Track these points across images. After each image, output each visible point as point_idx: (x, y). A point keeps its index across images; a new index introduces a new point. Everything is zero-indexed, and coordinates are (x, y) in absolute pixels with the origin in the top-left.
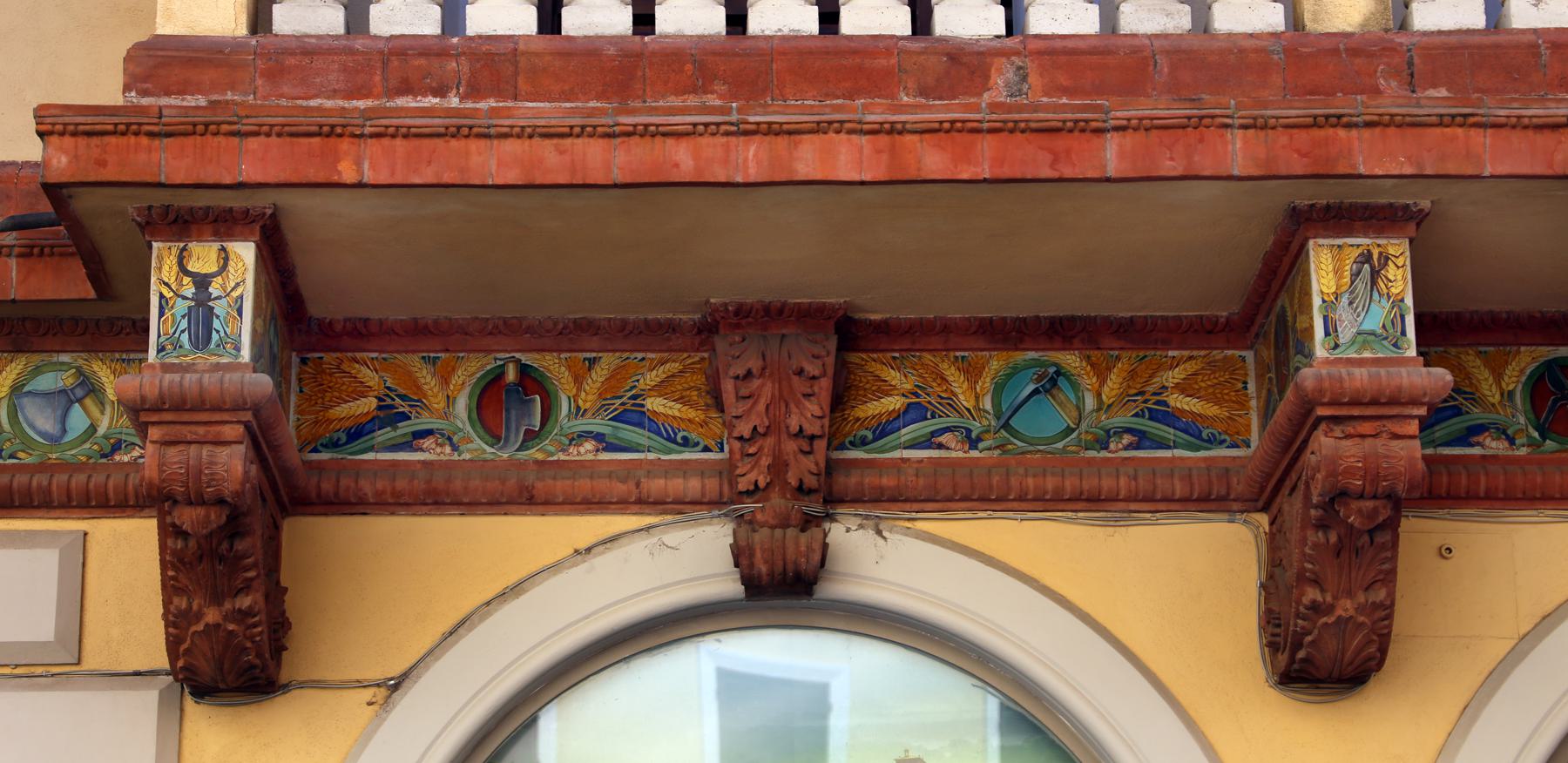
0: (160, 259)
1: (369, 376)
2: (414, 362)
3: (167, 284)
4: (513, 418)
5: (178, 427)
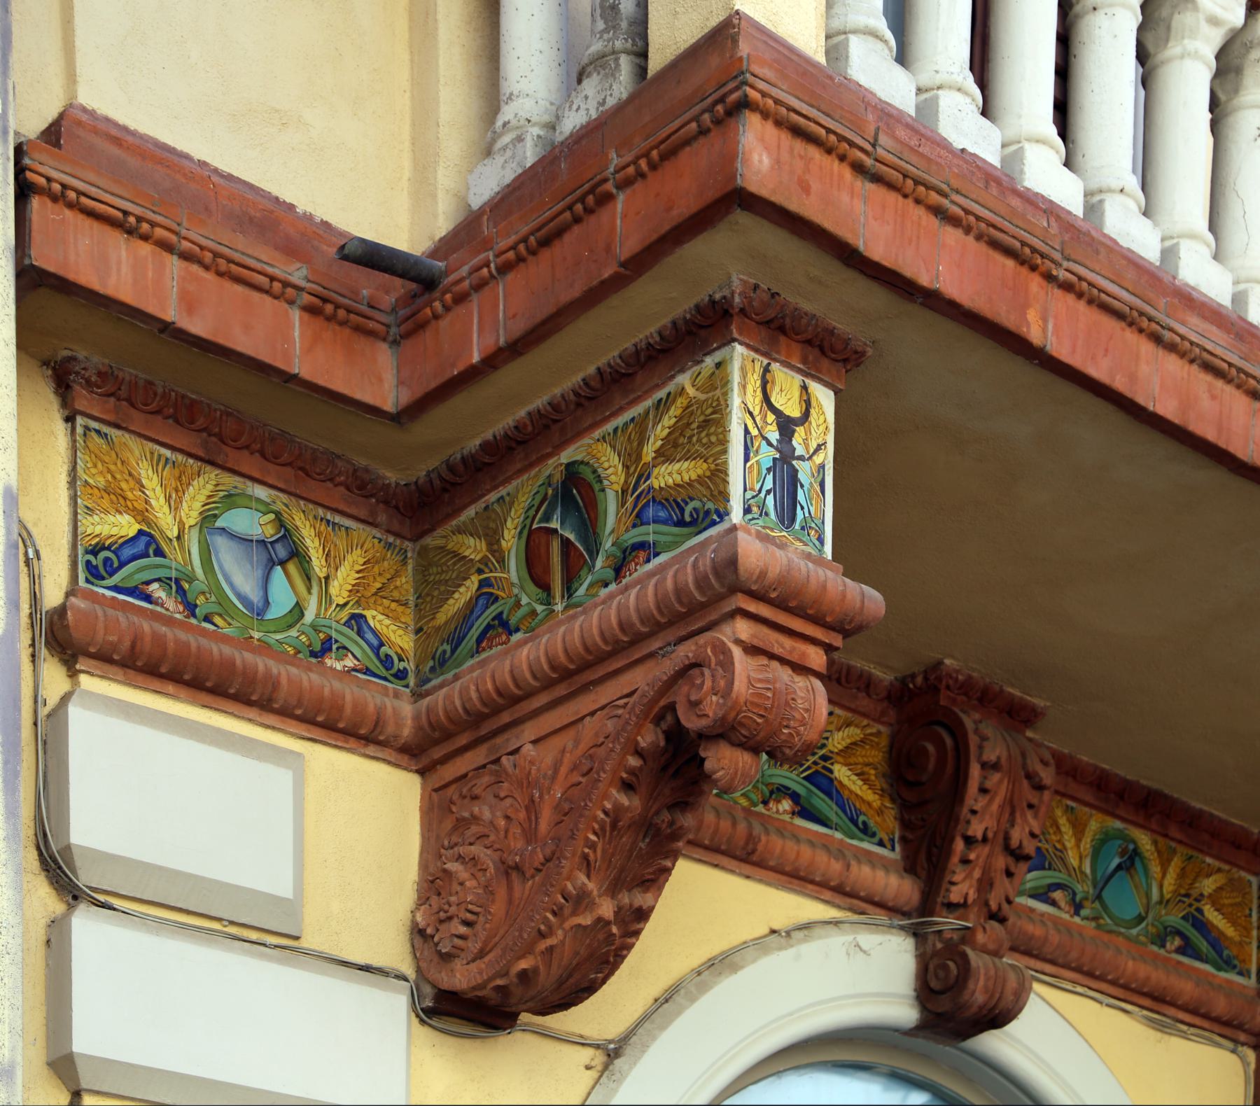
3: (751, 414)
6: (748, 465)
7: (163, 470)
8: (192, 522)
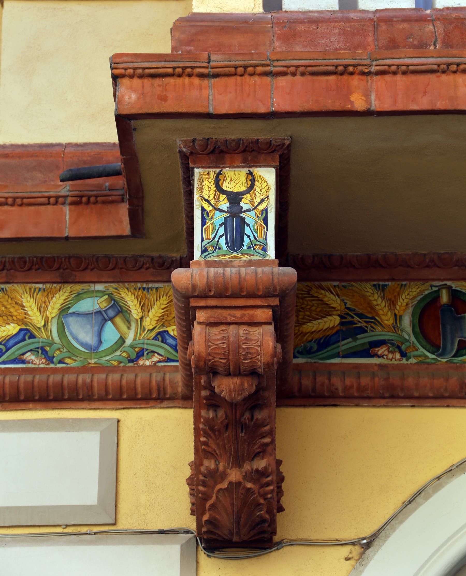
0: (201, 181)
1: (334, 301)
2: (368, 288)
3: (207, 201)
4: (449, 331)
5: (220, 311)
6: (205, 227)
7: (37, 295)
8: (53, 315)
